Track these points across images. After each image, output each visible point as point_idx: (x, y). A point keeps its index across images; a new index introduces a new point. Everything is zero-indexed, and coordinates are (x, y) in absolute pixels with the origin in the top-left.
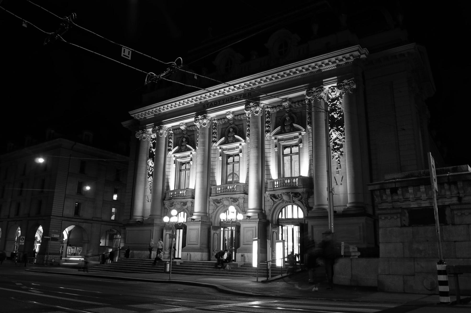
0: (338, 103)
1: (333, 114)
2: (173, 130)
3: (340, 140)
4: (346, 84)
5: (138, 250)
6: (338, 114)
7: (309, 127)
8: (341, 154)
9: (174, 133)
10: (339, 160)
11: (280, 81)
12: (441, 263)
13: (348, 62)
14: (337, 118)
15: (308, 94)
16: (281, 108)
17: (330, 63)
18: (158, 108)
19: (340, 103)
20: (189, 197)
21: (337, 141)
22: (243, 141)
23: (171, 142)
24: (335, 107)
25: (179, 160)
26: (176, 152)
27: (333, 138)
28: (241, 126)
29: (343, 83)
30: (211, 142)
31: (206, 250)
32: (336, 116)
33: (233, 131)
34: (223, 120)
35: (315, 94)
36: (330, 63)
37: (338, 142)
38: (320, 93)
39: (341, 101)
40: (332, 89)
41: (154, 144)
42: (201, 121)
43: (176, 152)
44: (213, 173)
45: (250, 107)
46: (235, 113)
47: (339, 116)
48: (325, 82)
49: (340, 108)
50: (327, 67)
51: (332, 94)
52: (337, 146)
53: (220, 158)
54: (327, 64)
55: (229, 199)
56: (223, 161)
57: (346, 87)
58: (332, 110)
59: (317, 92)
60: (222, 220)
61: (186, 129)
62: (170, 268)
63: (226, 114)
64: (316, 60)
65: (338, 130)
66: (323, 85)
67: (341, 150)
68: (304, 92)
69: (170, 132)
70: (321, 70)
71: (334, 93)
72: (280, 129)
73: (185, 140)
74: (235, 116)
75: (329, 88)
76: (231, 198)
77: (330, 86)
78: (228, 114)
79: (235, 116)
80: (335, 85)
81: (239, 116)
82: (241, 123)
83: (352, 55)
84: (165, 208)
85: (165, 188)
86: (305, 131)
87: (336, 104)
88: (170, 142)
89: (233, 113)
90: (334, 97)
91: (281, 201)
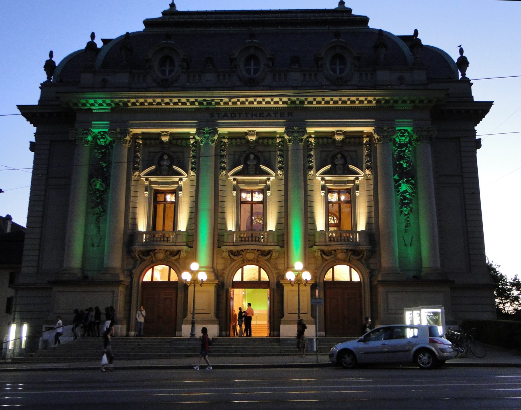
0: (407, 151)
1: (402, 162)
3: (410, 194)
4: (207, 133)
6: (407, 163)
8: (411, 211)
10: (408, 217)
13: (209, 108)
14: (406, 168)
15: (198, 133)
16: (330, 141)
17: (105, 105)
18: (126, 100)
19: (409, 151)
22: (274, 174)
24: (404, 154)
25: (329, 186)
27: (401, 191)
29: (204, 130)
30: (218, 169)
31: (125, 322)
32: (405, 166)
34: (238, 140)
36: (105, 105)
37: (408, 196)
38: (213, 136)
39: (410, 149)
40: (101, 135)
41: (104, 154)
42: (207, 136)
44: (312, 212)
47: (409, 166)
51: (102, 140)
53: (146, 194)
54: (404, 102)
55: (256, 251)
56: (150, 197)
57: (296, 135)
58: (402, 158)
59: (388, 132)
61: (170, 141)
62: (316, 348)
65: (408, 182)
67: (411, 205)
68: (193, 131)
70: (394, 107)
71: (104, 141)
72: (242, 168)
75: (99, 132)
76: (258, 250)
79: (174, 139)
80: (107, 130)
85: (130, 226)
87: (404, 151)
90: (103, 144)
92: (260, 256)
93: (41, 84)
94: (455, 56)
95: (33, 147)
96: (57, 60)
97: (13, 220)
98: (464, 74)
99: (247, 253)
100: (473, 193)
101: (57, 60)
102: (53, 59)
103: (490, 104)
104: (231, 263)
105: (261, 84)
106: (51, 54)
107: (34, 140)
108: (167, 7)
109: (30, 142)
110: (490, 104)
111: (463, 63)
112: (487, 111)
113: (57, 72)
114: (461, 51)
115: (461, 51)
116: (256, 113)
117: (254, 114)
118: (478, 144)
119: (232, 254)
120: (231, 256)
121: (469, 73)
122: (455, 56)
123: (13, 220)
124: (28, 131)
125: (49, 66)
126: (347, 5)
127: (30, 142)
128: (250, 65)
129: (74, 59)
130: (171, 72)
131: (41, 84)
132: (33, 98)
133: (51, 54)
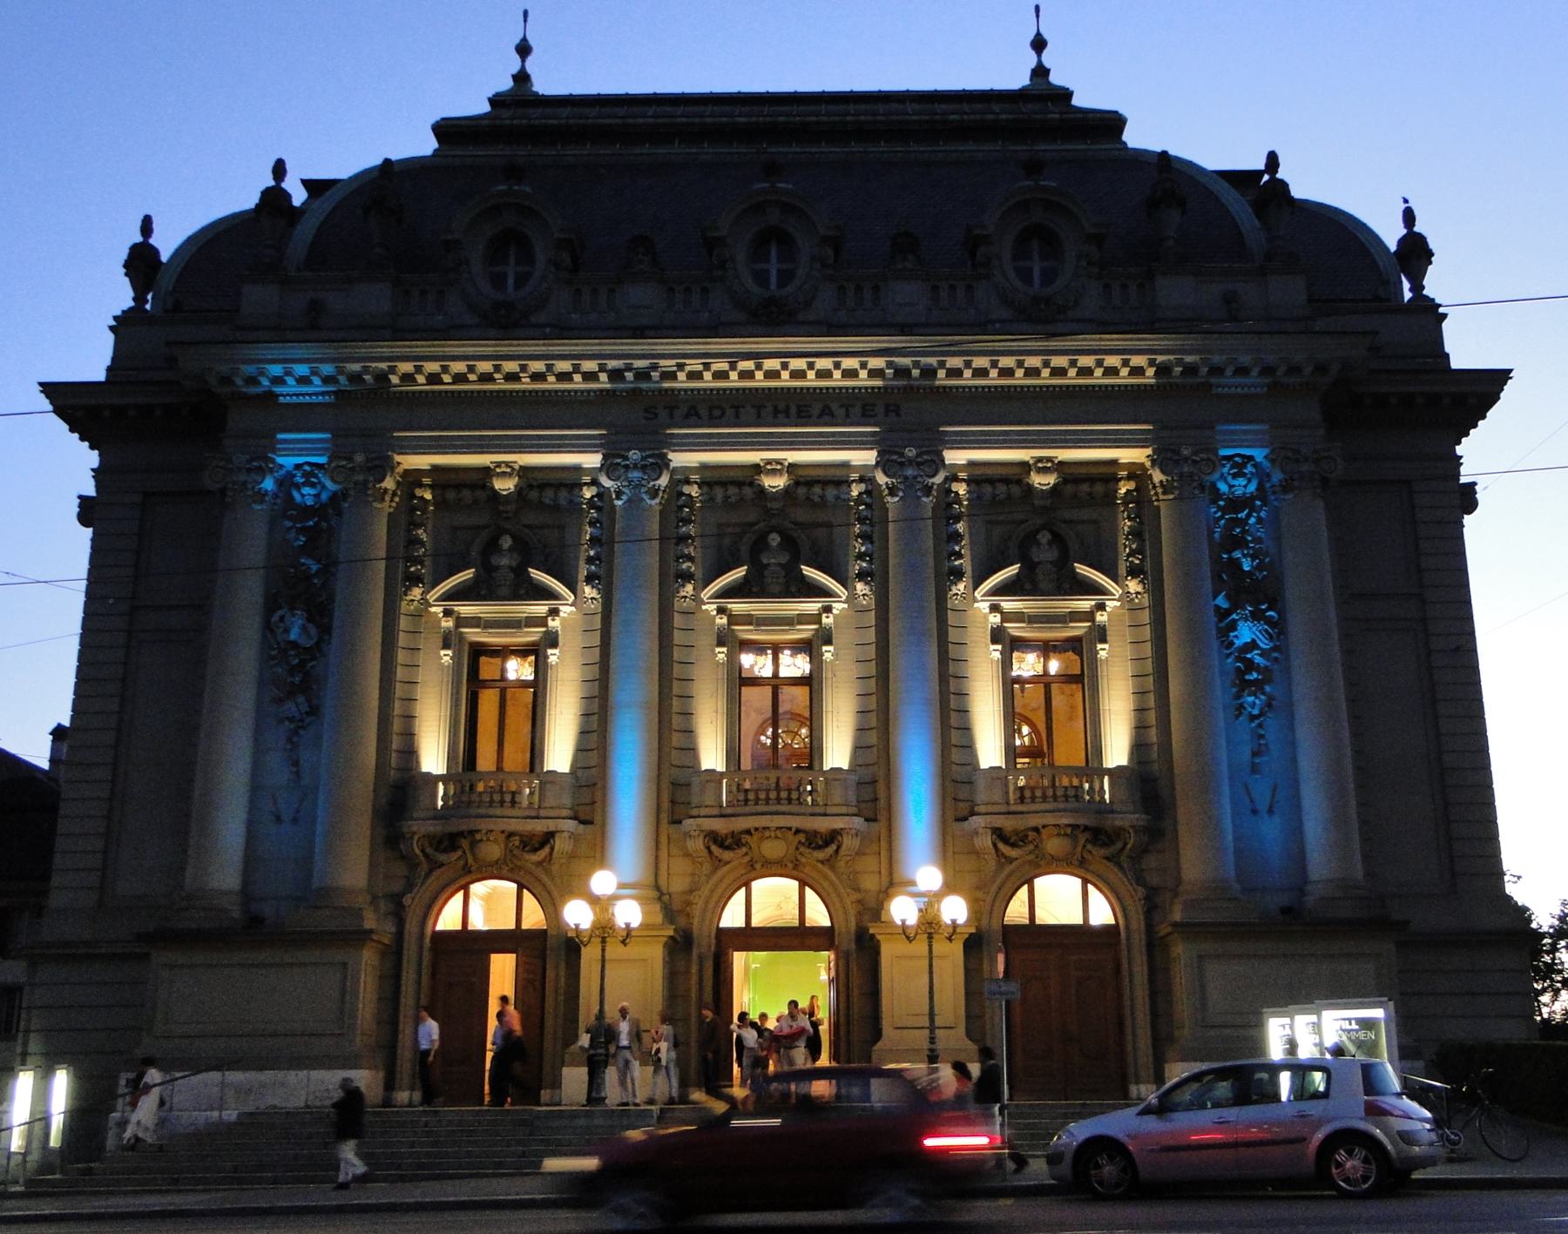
1: (1237, 554)
2: (968, 482)
3: (1263, 654)
5: (245, 1069)
7: (588, 591)
11: (316, 394)
18: (384, 366)
20: (565, 813)
21: (1255, 656)
23: (422, 543)
24: (1244, 532)
26: (1004, 590)
27: (1238, 643)
28: (821, 533)
30: (670, 579)
35: (910, 472)
37: (1258, 659)
39: (1263, 514)
40: (306, 475)
43: (1004, 590)
48: (285, 441)
49: (1257, 540)
50: (1239, 380)
52: (1255, 675)
53: (446, 656)
58: (1239, 543)
60: (1534, 925)
63: (757, 469)
65: (1257, 616)
66: (274, 451)
69: (686, 489)
70: (278, 396)
74: (531, 487)
75: (298, 467)
76: (798, 831)
77: (300, 460)
78: (774, 472)
79: (531, 487)
80: (322, 460)
81: (817, 490)
82: (821, 516)
83: (1152, 363)
85: (394, 760)
87: (1244, 522)
91: (1032, 857)
93: (115, 318)
94: (1391, 234)
95: (88, 511)
96: (166, 243)
98: (1417, 287)
99: (762, 839)
100: (1458, 649)
101: (166, 243)
103: (1503, 376)
105: (800, 317)
106: (147, 226)
108: (507, 84)
109: (80, 497)
111: (1415, 253)
112: (1493, 399)
113: (166, 281)
114: (1409, 217)
115: (1409, 217)
116: (788, 407)
118: (1467, 499)
121: (1434, 285)
122: (1391, 234)
124: (75, 464)
125: (141, 262)
126: (1056, 79)
127: (80, 497)
128: (768, 261)
129: (219, 243)
130: (521, 280)
131: (115, 318)
132: (90, 360)
133: (147, 226)
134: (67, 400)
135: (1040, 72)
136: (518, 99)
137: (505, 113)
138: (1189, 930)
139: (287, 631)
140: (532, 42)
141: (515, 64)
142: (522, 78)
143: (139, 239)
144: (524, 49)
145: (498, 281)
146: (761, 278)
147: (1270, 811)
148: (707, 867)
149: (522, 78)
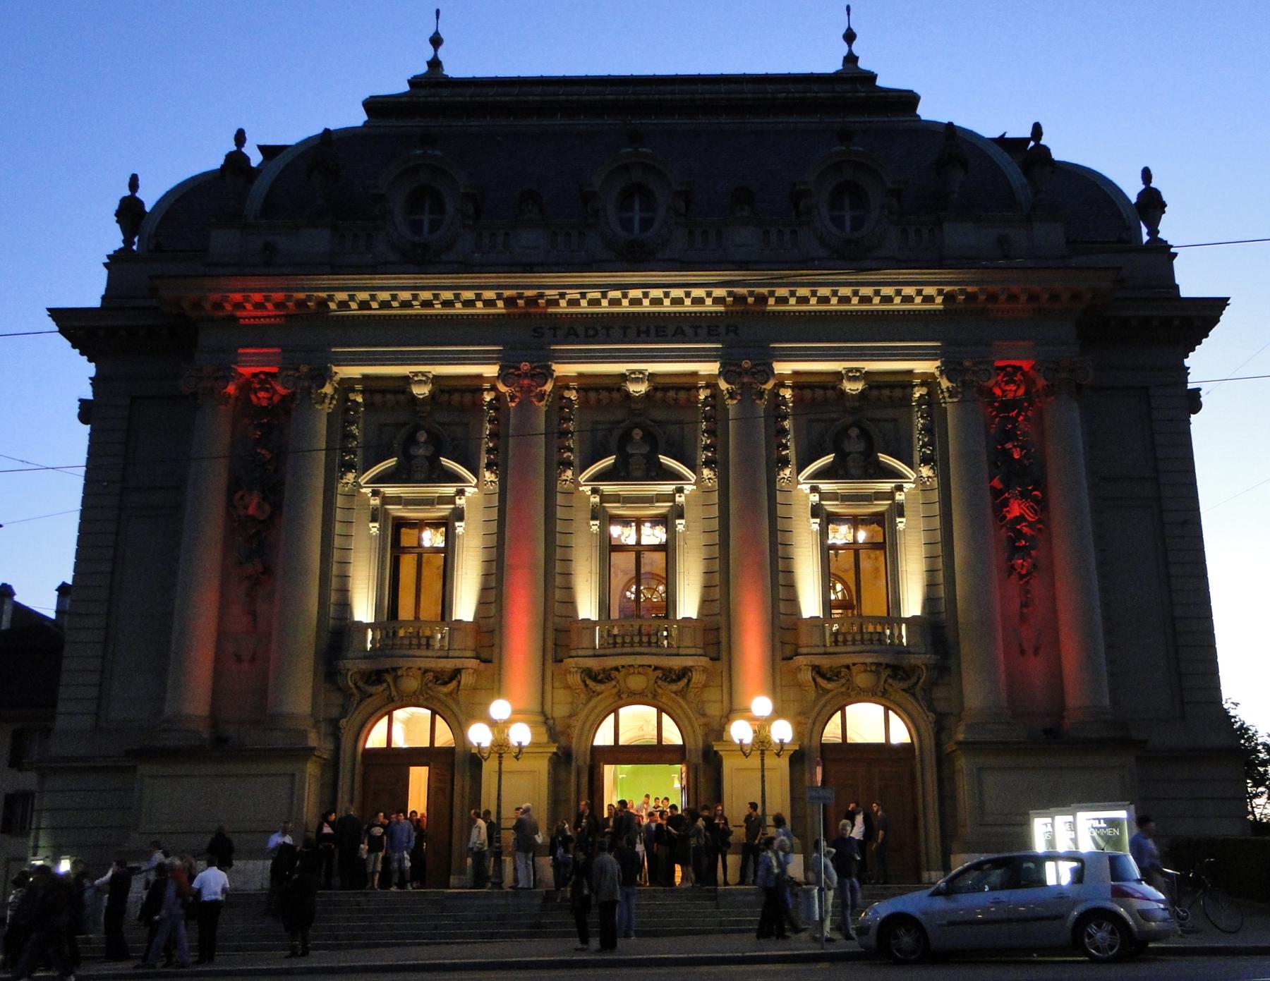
1: (1009, 446)
3: (1030, 525)
7: (489, 476)
9: (365, 404)
11: (269, 317)
12: (221, 854)
13: (530, 314)
19: (1027, 419)
23: (354, 437)
25: (396, 510)
27: (1009, 516)
33: (426, 442)
45: (740, 374)
46: (658, 380)
50: (259, 313)
53: (374, 528)
61: (433, 394)
64: (419, 282)
73: (423, 437)
74: (442, 391)
76: (656, 668)
84: (345, 692)
86: (476, 486)
87: (1015, 420)
88: (564, 434)
89: (437, 379)
92: (660, 682)
93: (109, 257)
94: (1132, 189)
95: (87, 412)
96: (150, 197)
97: (16, 598)
98: (1153, 232)
99: (628, 674)
101: (150, 197)
102: (1153, 185)
103: (1222, 303)
104: (590, 699)
105: (659, 255)
106: (134, 182)
107: (88, 394)
108: (422, 69)
109: (80, 400)
110: (1222, 303)
111: (1152, 204)
114: (1147, 175)
115: (1147, 175)
117: (643, 328)
118: (1193, 401)
119: (590, 677)
120: (588, 682)
122: (1132, 189)
123: (16, 598)
125: (129, 212)
126: (863, 64)
127: (80, 400)
131: (109, 257)
132: (89, 292)
133: (134, 182)
134: (71, 323)
135: (851, 59)
136: (432, 79)
137: (423, 92)
138: (970, 747)
139: (246, 507)
140: (443, 34)
141: (429, 53)
142: (435, 64)
143: (127, 193)
144: (436, 41)
145: (416, 226)
146: (627, 224)
147: (1036, 653)
148: (583, 697)
149: (435, 64)
